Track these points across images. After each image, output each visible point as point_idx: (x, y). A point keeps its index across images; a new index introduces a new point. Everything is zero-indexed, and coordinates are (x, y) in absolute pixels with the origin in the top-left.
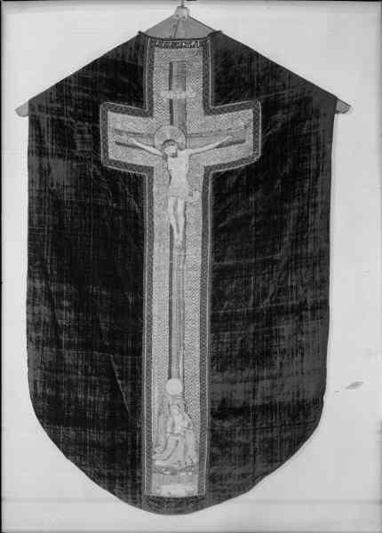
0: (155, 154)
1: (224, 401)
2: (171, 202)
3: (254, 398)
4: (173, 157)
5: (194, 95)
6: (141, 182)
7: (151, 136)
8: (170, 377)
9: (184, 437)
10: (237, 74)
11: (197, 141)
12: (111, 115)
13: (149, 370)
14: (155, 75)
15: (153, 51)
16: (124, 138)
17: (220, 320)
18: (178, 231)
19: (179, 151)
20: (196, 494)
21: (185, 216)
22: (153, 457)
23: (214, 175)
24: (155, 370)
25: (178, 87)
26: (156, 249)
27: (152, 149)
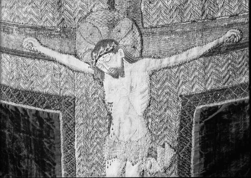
4: (116, 76)
19: (126, 63)
23: (205, 113)
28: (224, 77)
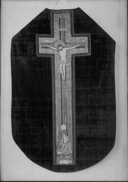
0: (55, 50)
1: (80, 136)
2: (61, 66)
3: (90, 135)
5: (68, 30)
6: (50, 60)
7: (54, 44)
8: (62, 124)
9: (67, 144)
10: (81, 22)
11: (69, 45)
12: (40, 39)
13: (55, 122)
14: (54, 23)
15: (53, 15)
16: (44, 46)
17: (78, 109)
18: (63, 75)
19: (63, 49)
20: (72, 164)
21: (66, 70)
22: (57, 151)
24: (57, 122)
25: (62, 27)
26: (56, 81)
27: (54, 48)
28: (64, 116)
